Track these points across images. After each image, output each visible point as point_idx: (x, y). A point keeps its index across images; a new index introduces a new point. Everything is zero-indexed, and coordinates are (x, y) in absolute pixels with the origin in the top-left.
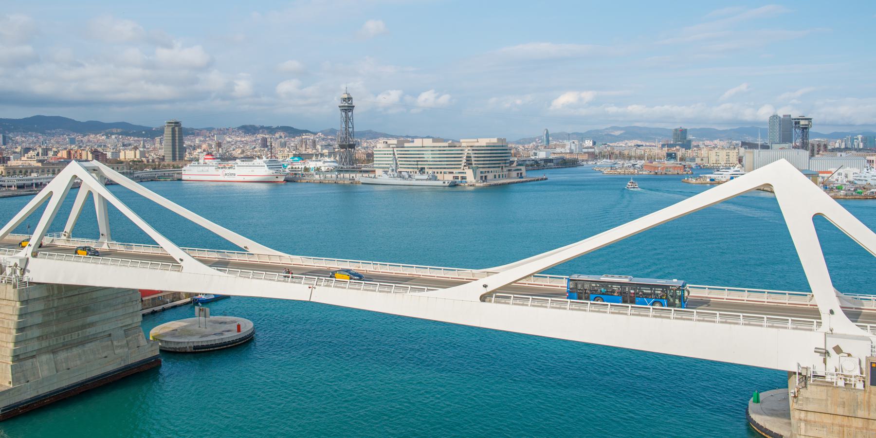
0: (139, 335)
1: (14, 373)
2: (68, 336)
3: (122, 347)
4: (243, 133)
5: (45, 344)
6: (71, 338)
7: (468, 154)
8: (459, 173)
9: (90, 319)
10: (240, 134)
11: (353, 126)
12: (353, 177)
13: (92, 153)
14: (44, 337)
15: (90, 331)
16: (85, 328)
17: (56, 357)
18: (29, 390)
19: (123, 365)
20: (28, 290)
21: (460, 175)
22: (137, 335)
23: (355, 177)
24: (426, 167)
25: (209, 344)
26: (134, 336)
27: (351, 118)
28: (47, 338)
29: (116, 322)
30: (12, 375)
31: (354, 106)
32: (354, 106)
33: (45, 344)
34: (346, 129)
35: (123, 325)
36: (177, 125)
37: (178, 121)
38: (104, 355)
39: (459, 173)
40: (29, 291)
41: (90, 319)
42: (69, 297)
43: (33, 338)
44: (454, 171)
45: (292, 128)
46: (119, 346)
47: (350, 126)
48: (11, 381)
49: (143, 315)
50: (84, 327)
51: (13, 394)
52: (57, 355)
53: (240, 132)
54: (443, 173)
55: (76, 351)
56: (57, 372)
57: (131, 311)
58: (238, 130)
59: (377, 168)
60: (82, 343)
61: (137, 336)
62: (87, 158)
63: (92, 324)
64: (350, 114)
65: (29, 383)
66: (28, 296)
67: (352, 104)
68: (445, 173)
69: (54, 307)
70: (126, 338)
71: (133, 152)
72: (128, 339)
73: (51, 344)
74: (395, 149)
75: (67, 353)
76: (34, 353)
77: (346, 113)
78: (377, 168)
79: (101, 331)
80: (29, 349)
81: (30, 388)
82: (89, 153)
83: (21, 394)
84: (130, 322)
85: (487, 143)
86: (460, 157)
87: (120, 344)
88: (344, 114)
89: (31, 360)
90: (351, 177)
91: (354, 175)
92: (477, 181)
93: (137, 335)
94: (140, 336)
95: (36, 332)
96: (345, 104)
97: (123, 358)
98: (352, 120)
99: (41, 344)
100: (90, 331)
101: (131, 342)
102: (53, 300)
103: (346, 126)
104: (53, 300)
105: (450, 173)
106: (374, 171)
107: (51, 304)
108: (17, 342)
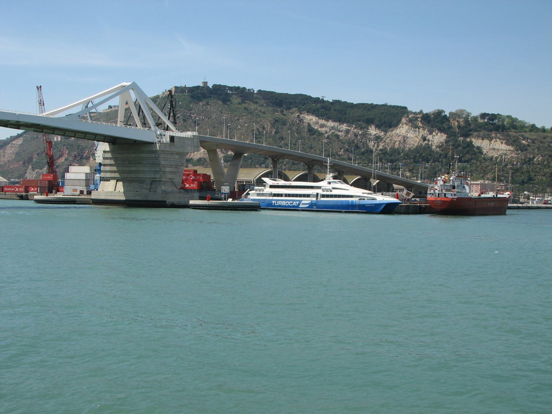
3: (146, 189)
19: (145, 199)
41: (142, 169)
49: (152, 181)
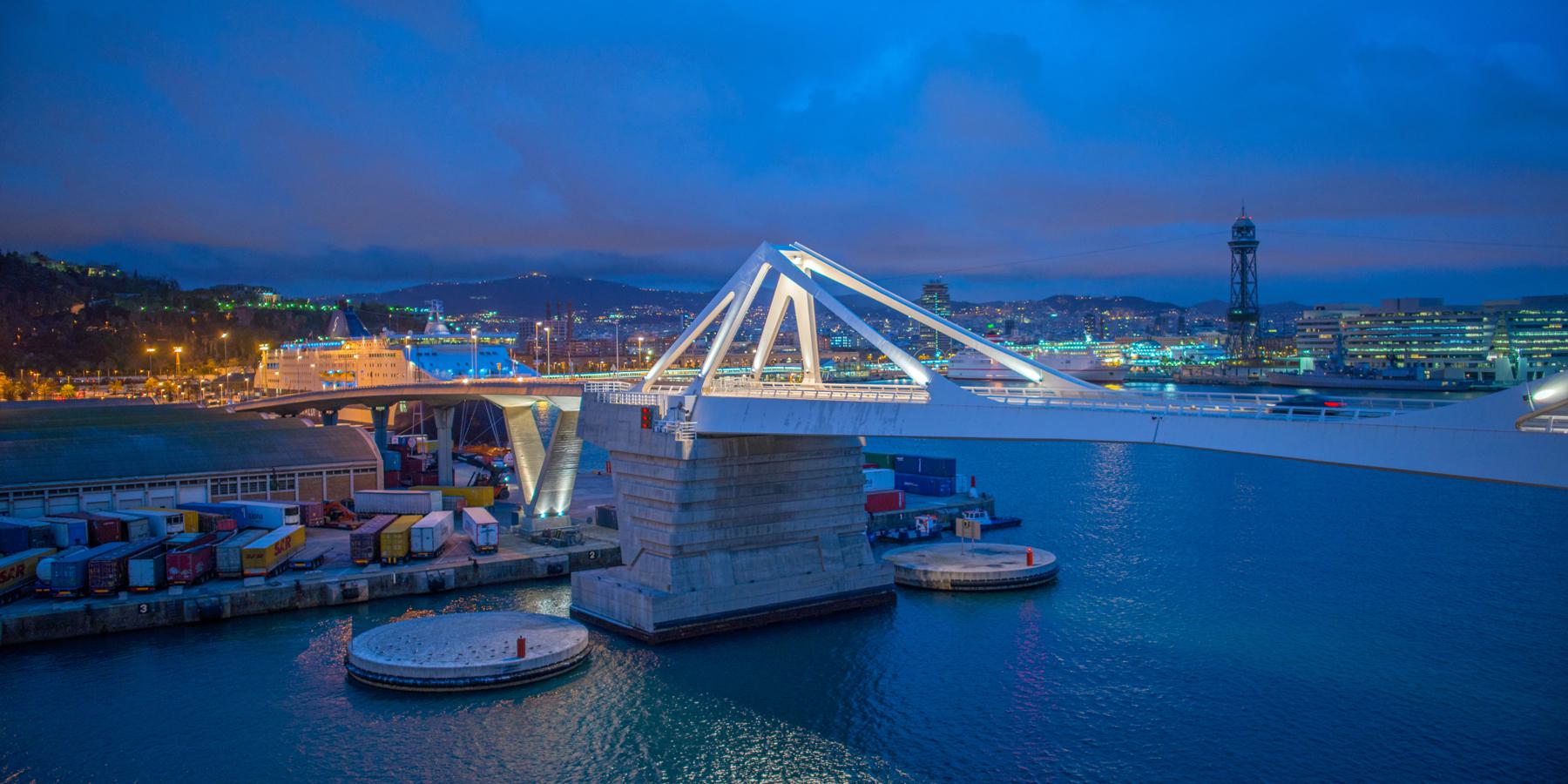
9: (786, 507)
15: (786, 526)
18: (695, 604)
25: (978, 578)
31: (1258, 242)
32: (1258, 242)
33: (719, 535)
38: (806, 570)
41: (786, 507)
42: (755, 464)
50: (778, 517)
55: (764, 555)
56: (736, 583)
60: (774, 543)
61: (859, 547)
63: (788, 516)
65: (695, 593)
67: (1254, 236)
69: (733, 478)
70: (842, 547)
72: (844, 549)
89: (699, 558)
94: (864, 549)
98: (1253, 269)
100: (786, 526)
101: (850, 556)
102: (732, 466)
104: (732, 466)
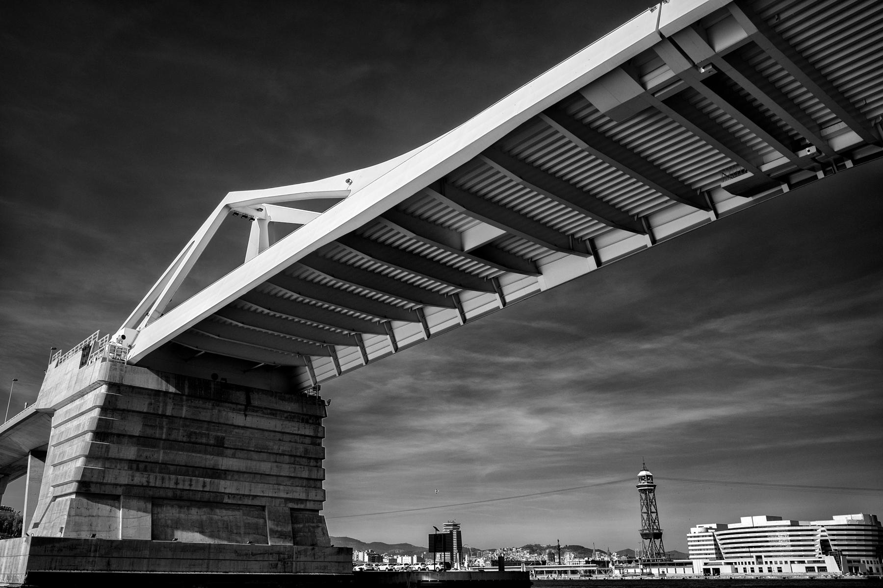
0: (318, 527)
1: (73, 513)
2: (184, 481)
4: (528, 554)
5: (139, 479)
6: (191, 485)
7: (822, 536)
8: (815, 562)
9: (226, 463)
10: (524, 554)
11: (656, 510)
12: (663, 572)
13: (368, 554)
14: (142, 466)
16: (219, 478)
17: (158, 513)
20: (124, 369)
21: (816, 565)
22: (314, 525)
23: (666, 572)
24: (763, 554)
26: (307, 525)
27: (653, 501)
28: (145, 470)
29: (276, 486)
30: (69, 515)
33: (139, 479)
34: (648, 514)
35: (288, 496)
36: (456, 527)
37: (456, 523)
39: (815, 562)
40: (126, 372)
41: (226, 463)
43: (121, 460)
44: (806, 559)
45: (583, 547)
46: (277, 531)
47: (654, 510)
48: (64, 526)
51: (60, 550)
52: (159, 510)
53: (525, 552)
54: (789, 563)
57: (305, 474)
58: (522, 550)
59: (694, 559)
61: (313, 527)
62: (364, 560)
64: (651, 495)
66: (122, 378)
68: (792, 562)
71: (410, 557)
72: (296, 526)
73: (152, 484)
74: (716, 533)
75: (180, 513)
76: (119, 491)
77: (646, 494)
78: (694, 559)
79: (247, 493)
80: (110, 478)
81: (95, 551)
82: (366, 555)
83: (75, 556)
84: (303, 496)
85: (848, 521)
86: (813, 540)
87: (279, 529)
88: (643, 496)
90: (661, 573)
91: (665, 570)
92: (844, 573)
93: (314, 525)
94: (320, 529)
95: (130, 452)
96: (644, 483)
97: (282, 556)
99: (133, 476)
103: (648, 511)
105: (800, 562)
106: (691, 563)
107: (161, 409)
108: (91, 457)
